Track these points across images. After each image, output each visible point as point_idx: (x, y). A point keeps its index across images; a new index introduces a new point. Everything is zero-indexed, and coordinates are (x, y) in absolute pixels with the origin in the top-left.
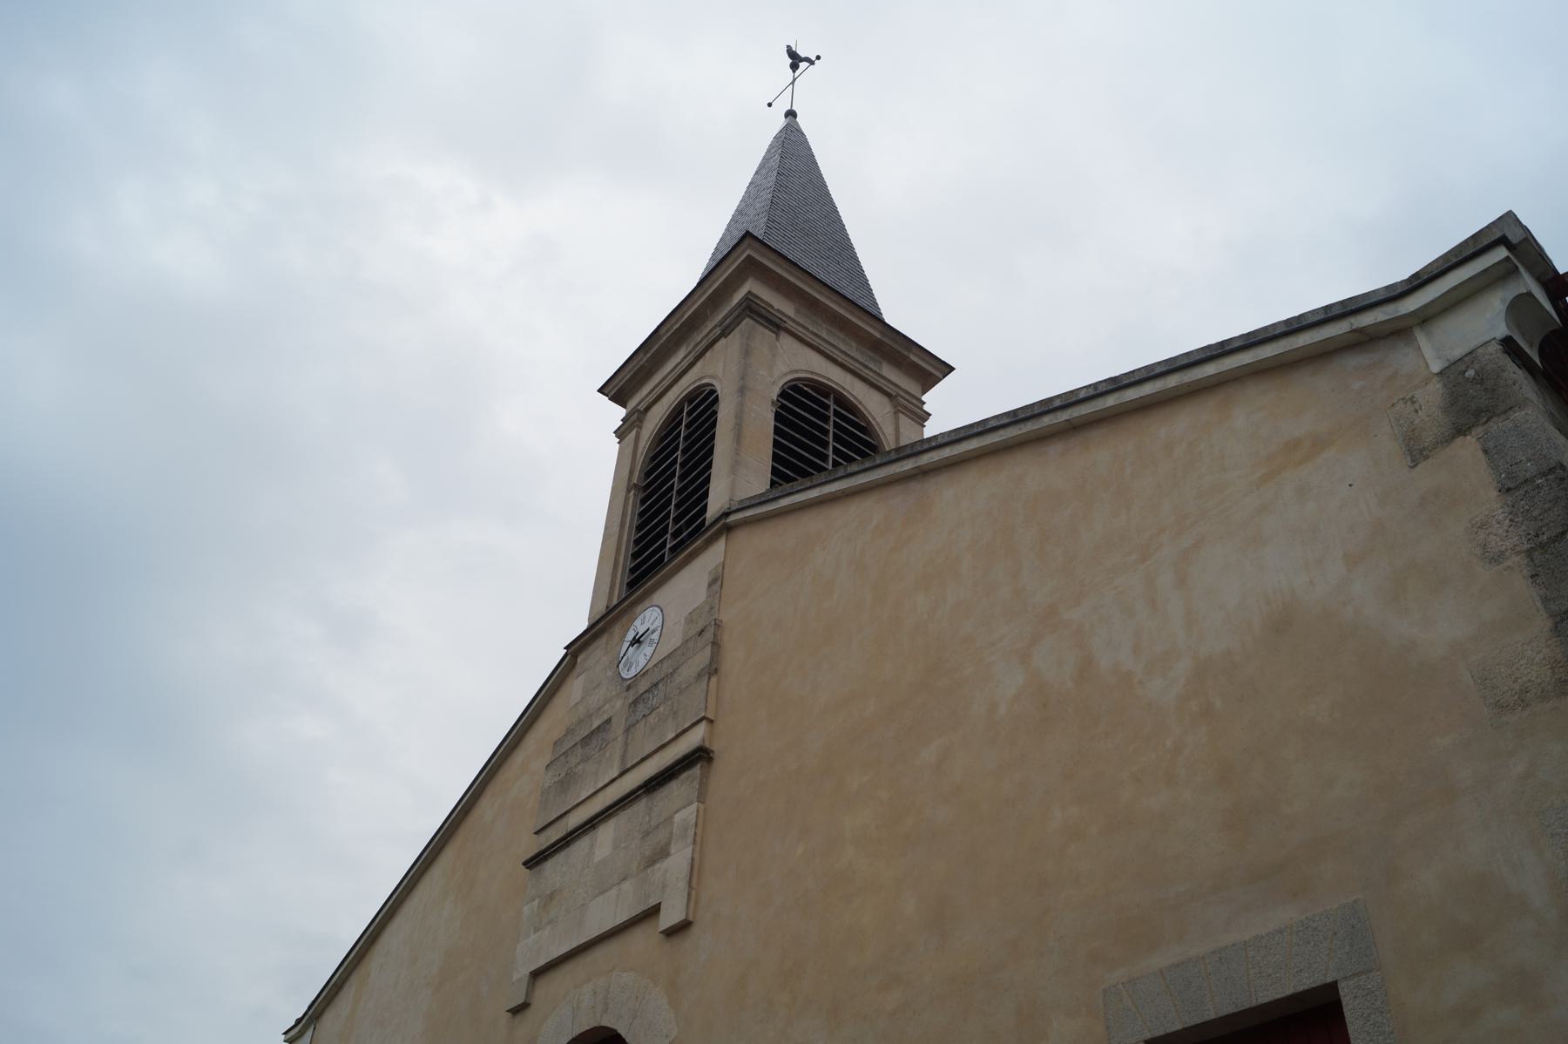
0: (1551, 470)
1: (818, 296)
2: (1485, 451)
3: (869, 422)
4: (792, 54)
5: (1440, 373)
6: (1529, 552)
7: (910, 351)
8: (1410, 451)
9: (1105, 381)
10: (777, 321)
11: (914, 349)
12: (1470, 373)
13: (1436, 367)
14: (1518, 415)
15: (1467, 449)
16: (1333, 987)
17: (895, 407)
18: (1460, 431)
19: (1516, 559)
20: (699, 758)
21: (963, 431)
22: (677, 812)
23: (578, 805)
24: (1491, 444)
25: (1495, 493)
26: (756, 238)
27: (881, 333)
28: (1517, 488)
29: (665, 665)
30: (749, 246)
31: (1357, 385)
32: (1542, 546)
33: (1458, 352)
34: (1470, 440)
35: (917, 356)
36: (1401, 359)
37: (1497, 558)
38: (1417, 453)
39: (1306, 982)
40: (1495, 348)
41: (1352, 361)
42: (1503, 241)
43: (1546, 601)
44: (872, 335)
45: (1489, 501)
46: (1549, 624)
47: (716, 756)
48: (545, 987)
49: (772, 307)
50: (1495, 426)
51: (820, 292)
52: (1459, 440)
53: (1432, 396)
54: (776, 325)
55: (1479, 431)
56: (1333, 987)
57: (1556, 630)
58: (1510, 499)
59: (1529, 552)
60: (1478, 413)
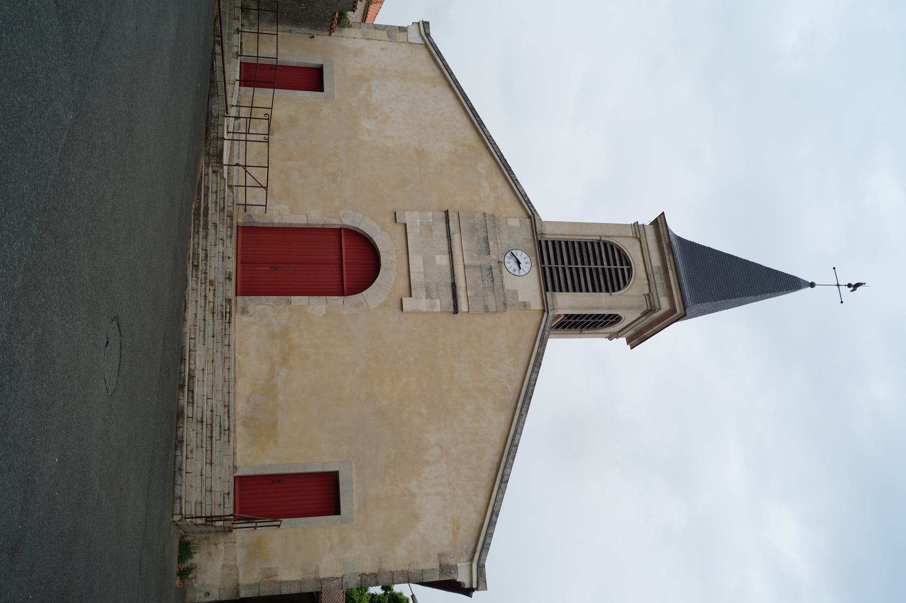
1: (661, 324)
3: (605, 327)
5: (456, 565)
6: (408, 571)
7: (639, 340)
8: (441, 554)
9: (508, 479)
12: (453, 571)
13: (458, 565)
16: (340, 514)
18: (440, 565)
21: (522, 425)
22: (440, 301)
24: (434, 570)
28: (422, 573)
29: (499, 283)
30: (681, 313)
31: (465, 546)
34: (438, 566)
36: (466, 558)
37: (410, 565)
43: (397, 571)
46: (392, 571)
48: (400, 228)
51: (662, 325)
53: (452, 562)
54: (645, 314)
55: (439, 568)
56: (340, 514)
58: (421, 571)
59: (408, 571)
60: (442, 570)
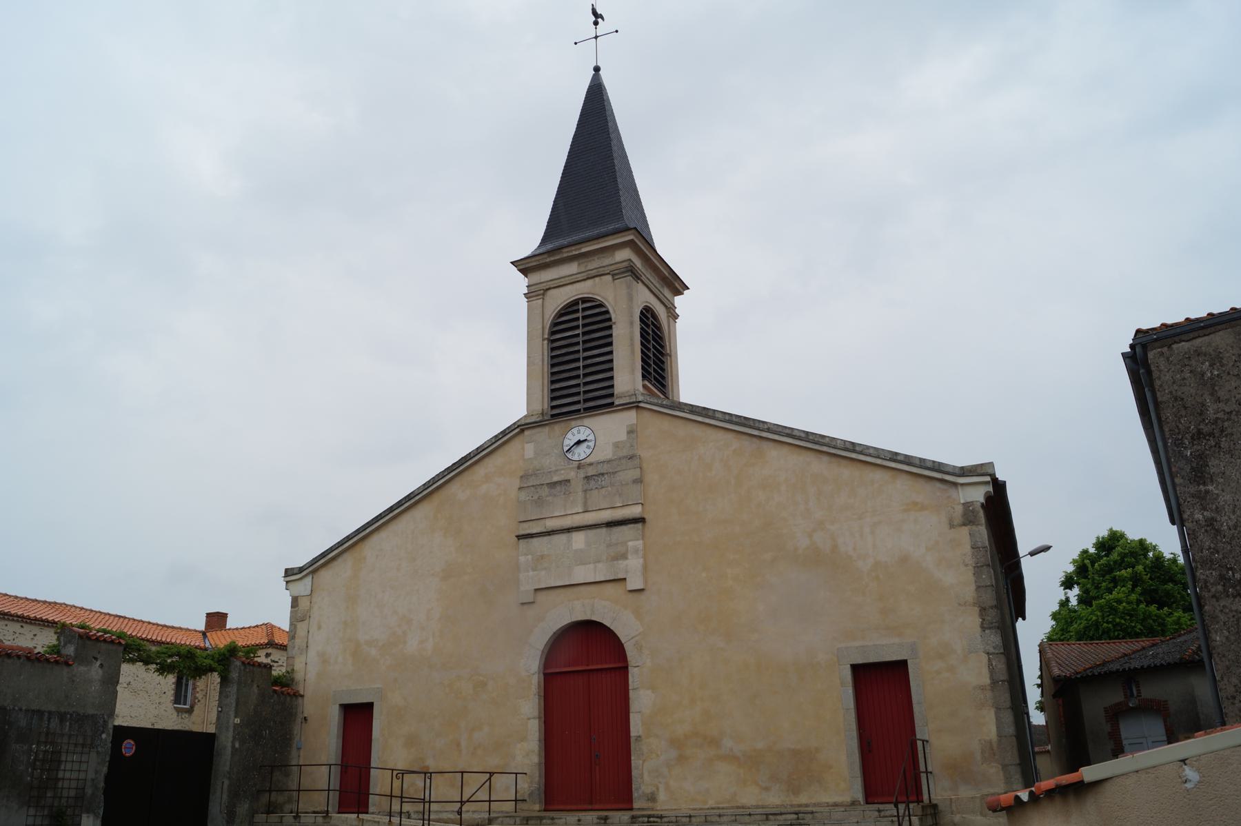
0: (985, 547)
2: (970, 534)
3: (660, 324)
4: (595, 13)
5: (963, 504)
6: (975, 567)
8: (950, 524)
10: (639, 276)
11: (678, 280)
13: (962, 501)
14: (980, 527)
15: (965, 531)
17: (668, 313)
18: (964, 524)
19: (971, 567)
20: (641, 522)
23: (552, 517)
25: (969, 547)
26: (637, 230)
27: (669, 274)
32: (978, 567)
33: (969, 500)
35: (678, 284)
37: (967, 565)
38: (952, 526)
39: (899, 658)
40: (979, 504)
41: (938, 485)
42: (990, 475)
43: (976, 582)
44: (665, 274)
45: (967, 548)
47: (646, 520)
48: (542, 597)
49: (636, 266)
50: (974, 528)
52: (963, 527)
55: (969, 526)
57: (976, 590)
59: (975, 567)
60: (970, 522)
